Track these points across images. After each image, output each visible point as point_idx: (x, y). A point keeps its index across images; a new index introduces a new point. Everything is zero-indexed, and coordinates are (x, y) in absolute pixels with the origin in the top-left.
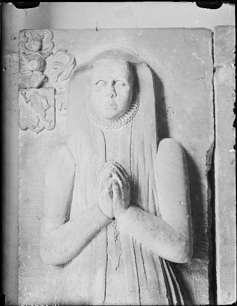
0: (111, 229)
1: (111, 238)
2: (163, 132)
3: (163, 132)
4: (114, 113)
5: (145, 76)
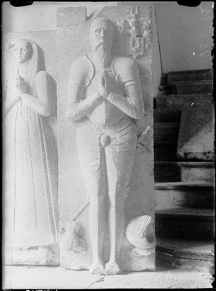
0: (19, 102)
1: (19, 105)
2: (41, 67)
3: (41, 67)
4: (22, 60)
5: (34, 47)
